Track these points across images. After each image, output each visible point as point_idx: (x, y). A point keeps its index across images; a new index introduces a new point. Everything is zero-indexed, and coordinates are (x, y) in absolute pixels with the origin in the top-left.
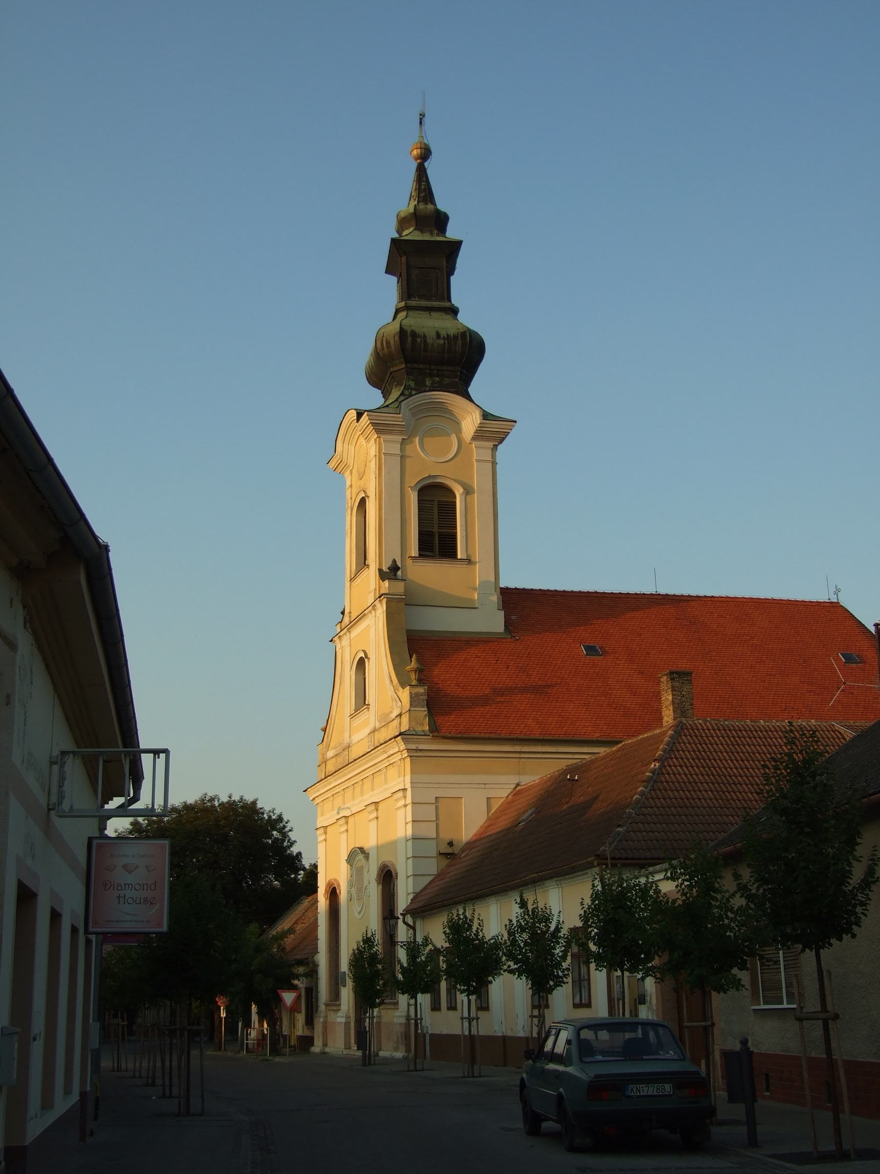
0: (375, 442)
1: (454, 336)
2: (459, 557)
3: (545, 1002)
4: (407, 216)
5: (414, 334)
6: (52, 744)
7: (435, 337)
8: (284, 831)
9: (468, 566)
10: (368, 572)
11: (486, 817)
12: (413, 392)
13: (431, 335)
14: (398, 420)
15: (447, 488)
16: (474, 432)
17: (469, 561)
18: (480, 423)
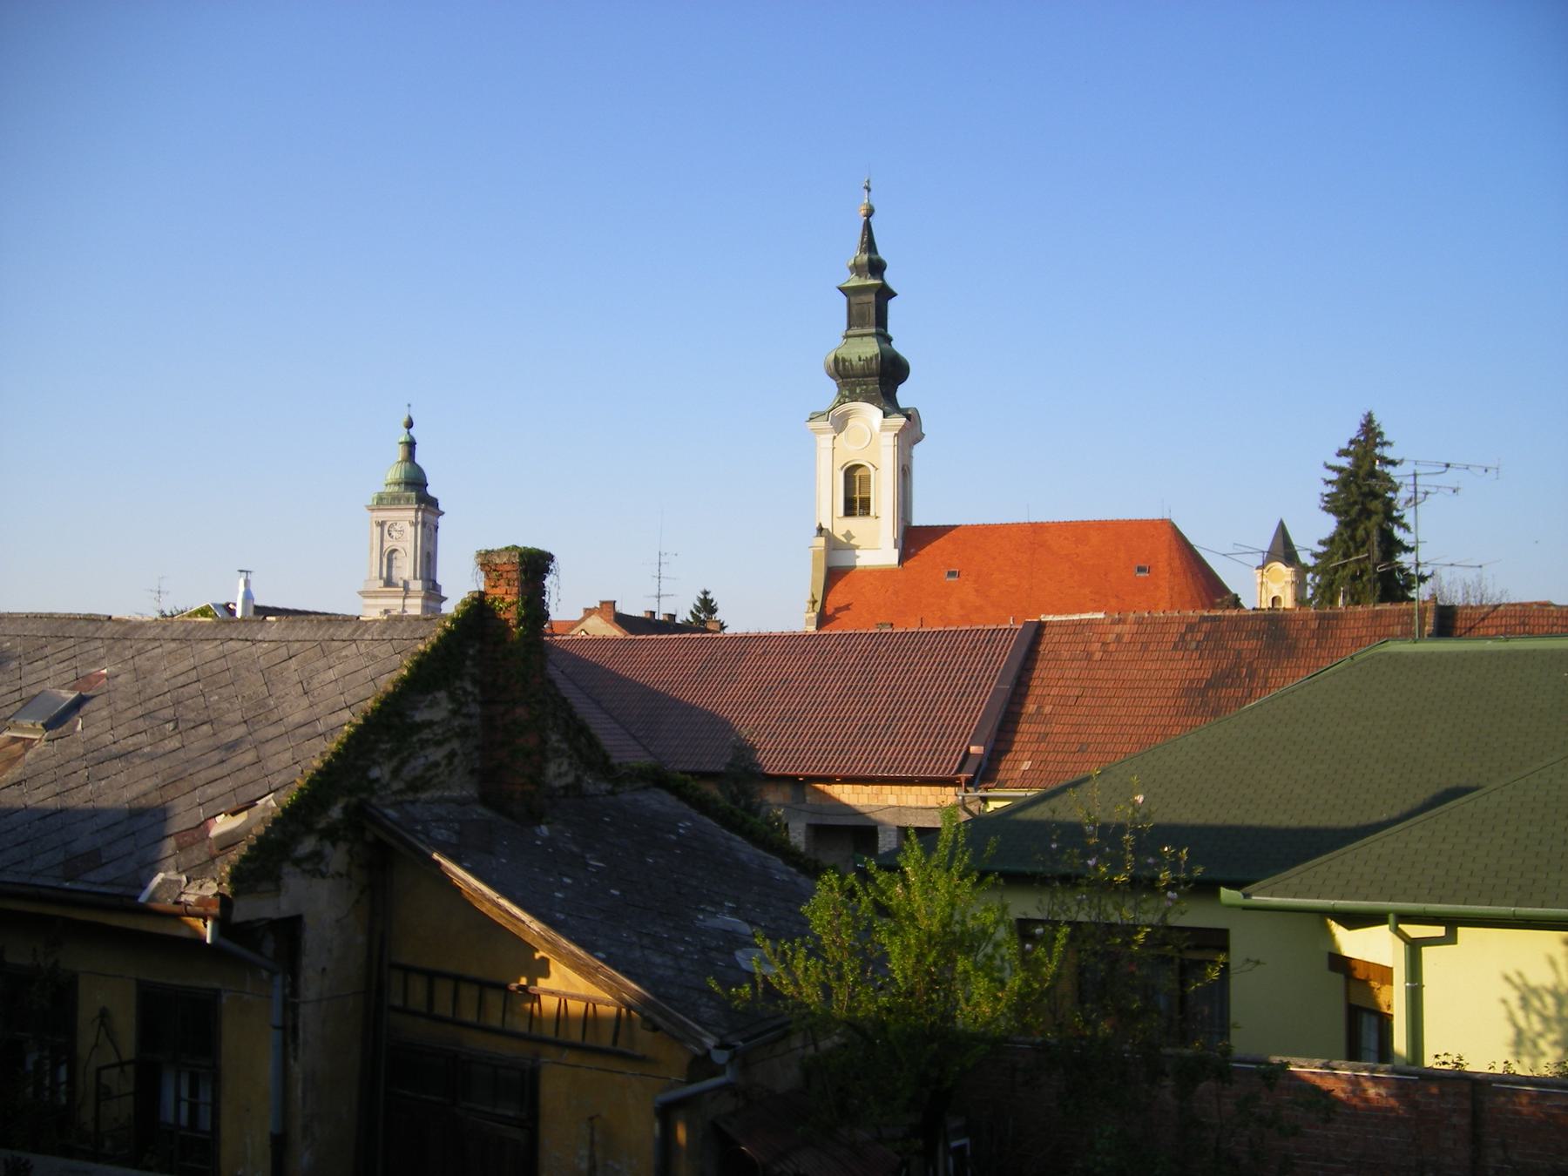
3: (1185, 945)
5: (844, 360)
6: (565, 1065)
7: (857, 359)
8: (454, 840)
11: (772, 763)
12: (847, 400)
13: (855, 360)
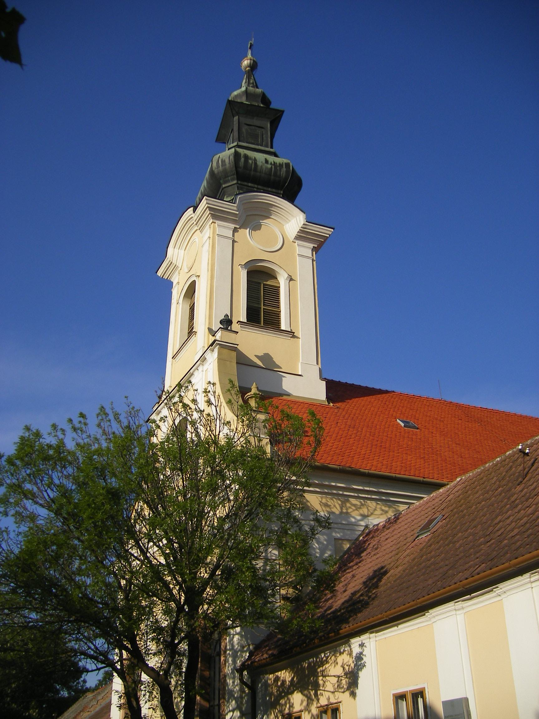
0: (210, 228)
1: (279, 164)
2: (283, 327)
4: (239, 94)
7: (264, 161)
9: (292, 339)
10: (195, 338)
14: (232, 208)
15: (271, 275)
16: (298, 230)
17: (292, 334)
18: (304, 224)
